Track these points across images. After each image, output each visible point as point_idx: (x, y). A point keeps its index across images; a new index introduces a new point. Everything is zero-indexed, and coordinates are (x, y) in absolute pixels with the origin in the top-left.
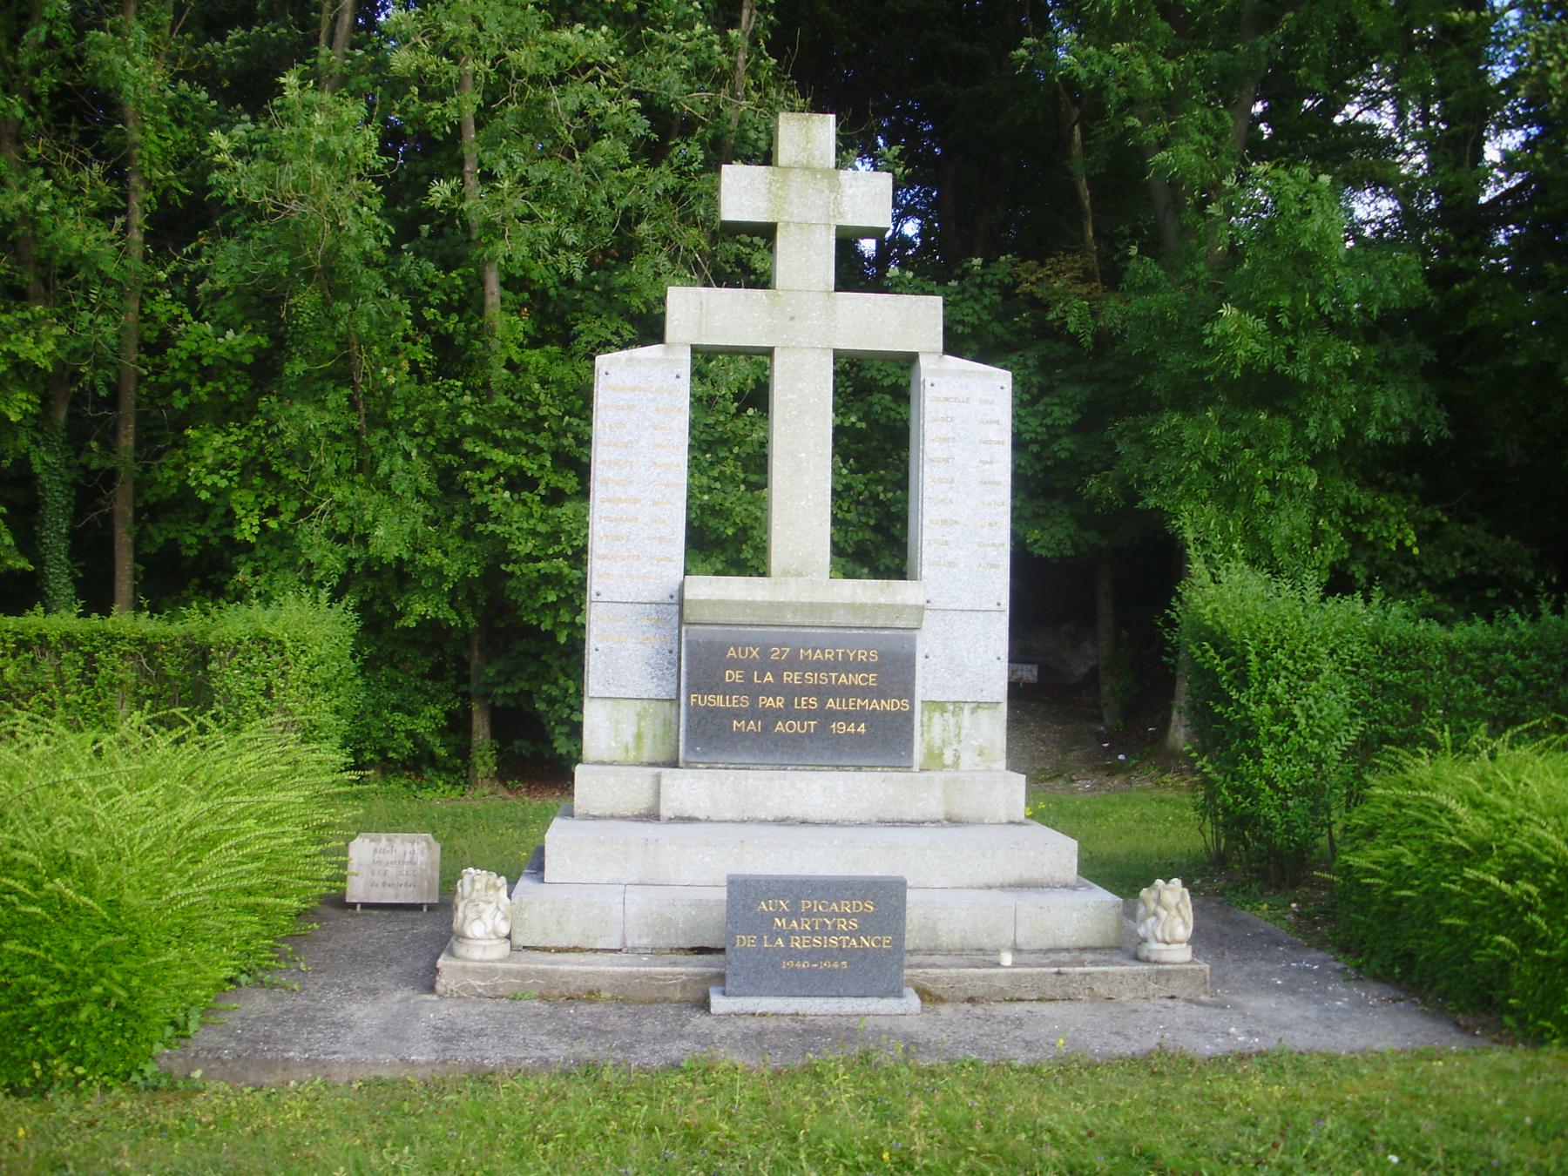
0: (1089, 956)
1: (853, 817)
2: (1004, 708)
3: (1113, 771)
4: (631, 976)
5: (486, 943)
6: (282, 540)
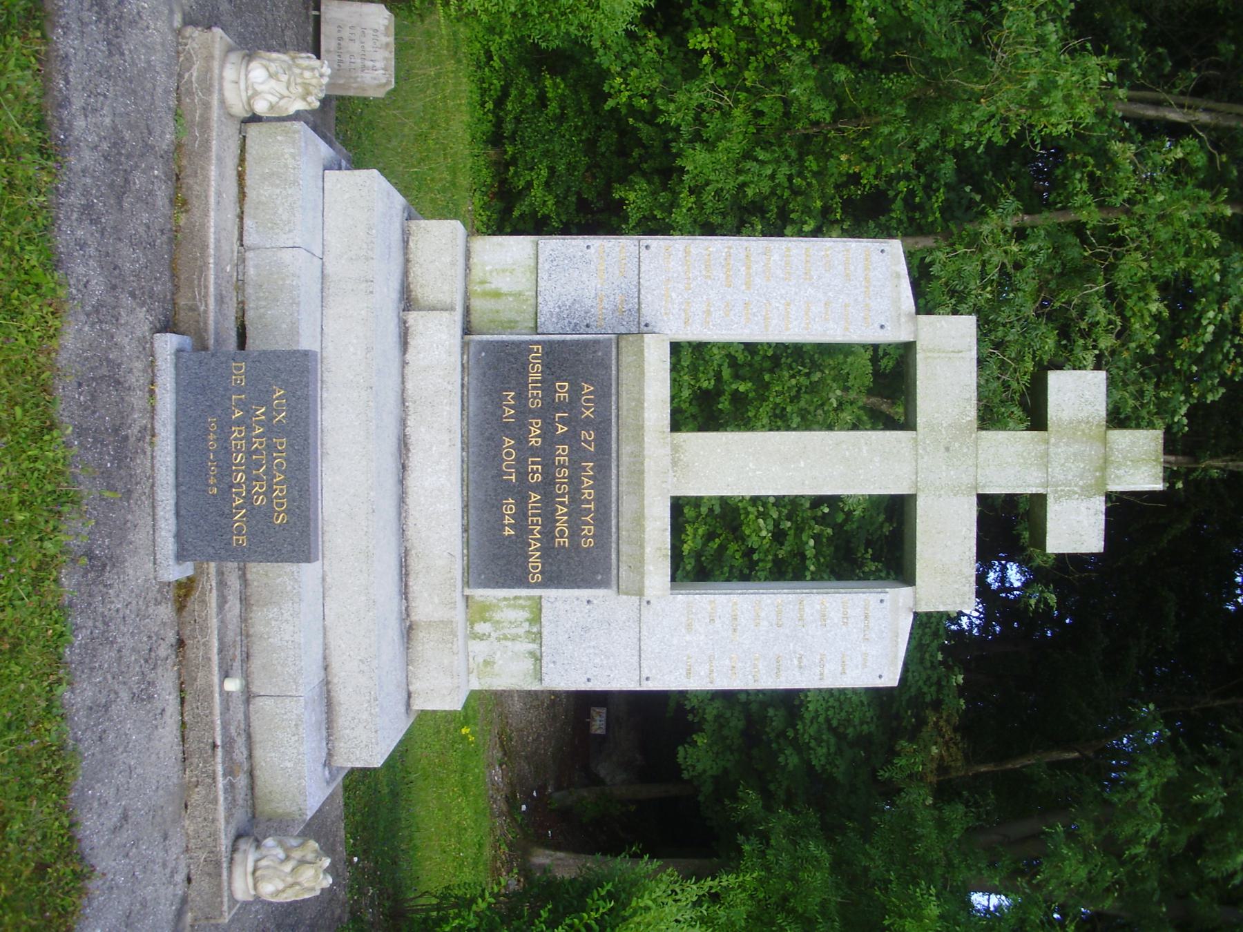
0: (242, 781)
1: (411, 521)
2: (536, 687)
3: (511, 801)
4: (205, 247)
5: (242, 86)
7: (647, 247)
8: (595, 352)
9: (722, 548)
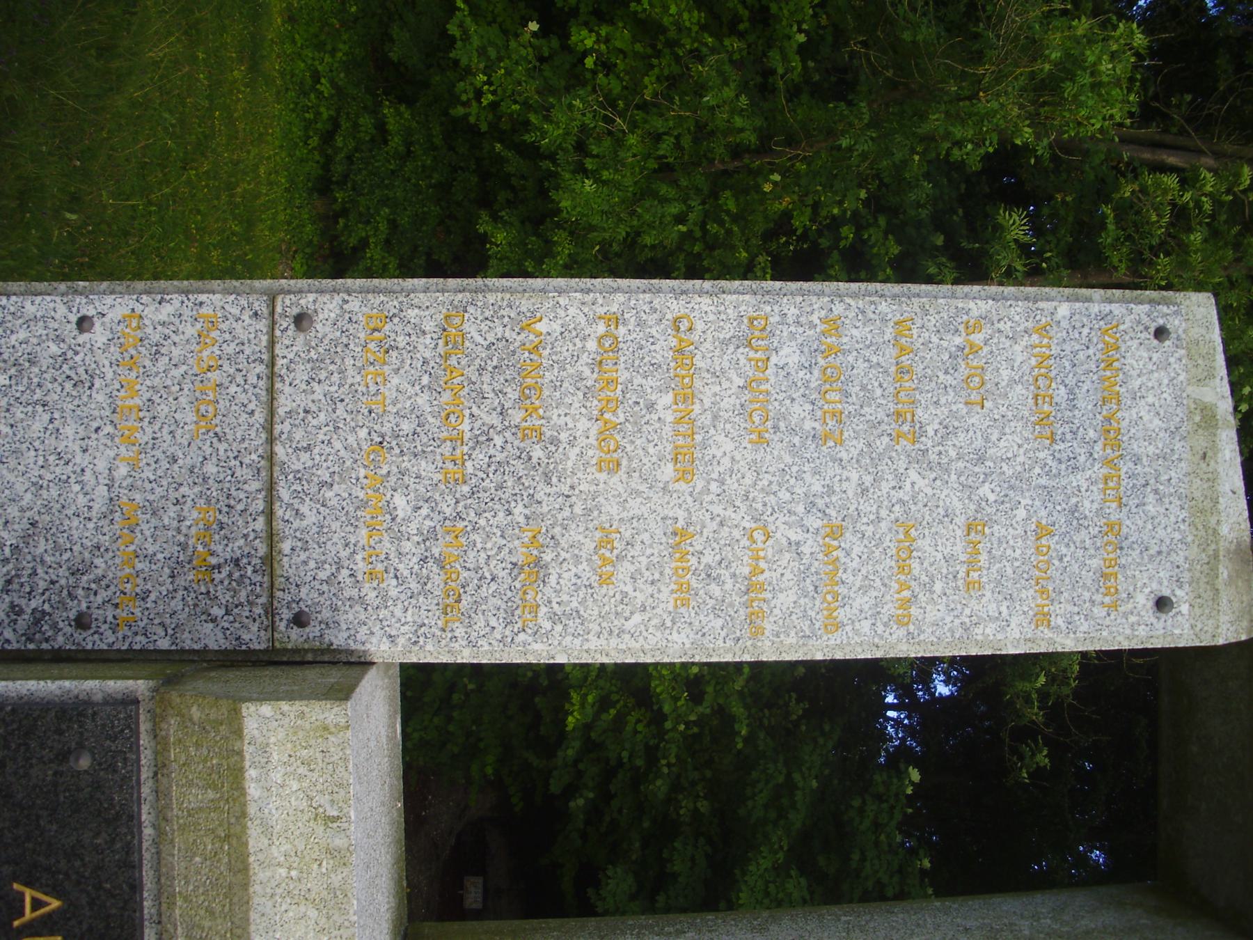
6: (576, 78)
7: (301, 321)
8: (64, 756)
9: (620, 720)
